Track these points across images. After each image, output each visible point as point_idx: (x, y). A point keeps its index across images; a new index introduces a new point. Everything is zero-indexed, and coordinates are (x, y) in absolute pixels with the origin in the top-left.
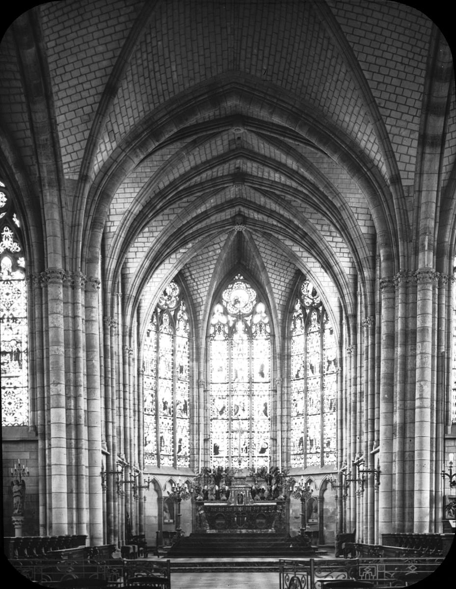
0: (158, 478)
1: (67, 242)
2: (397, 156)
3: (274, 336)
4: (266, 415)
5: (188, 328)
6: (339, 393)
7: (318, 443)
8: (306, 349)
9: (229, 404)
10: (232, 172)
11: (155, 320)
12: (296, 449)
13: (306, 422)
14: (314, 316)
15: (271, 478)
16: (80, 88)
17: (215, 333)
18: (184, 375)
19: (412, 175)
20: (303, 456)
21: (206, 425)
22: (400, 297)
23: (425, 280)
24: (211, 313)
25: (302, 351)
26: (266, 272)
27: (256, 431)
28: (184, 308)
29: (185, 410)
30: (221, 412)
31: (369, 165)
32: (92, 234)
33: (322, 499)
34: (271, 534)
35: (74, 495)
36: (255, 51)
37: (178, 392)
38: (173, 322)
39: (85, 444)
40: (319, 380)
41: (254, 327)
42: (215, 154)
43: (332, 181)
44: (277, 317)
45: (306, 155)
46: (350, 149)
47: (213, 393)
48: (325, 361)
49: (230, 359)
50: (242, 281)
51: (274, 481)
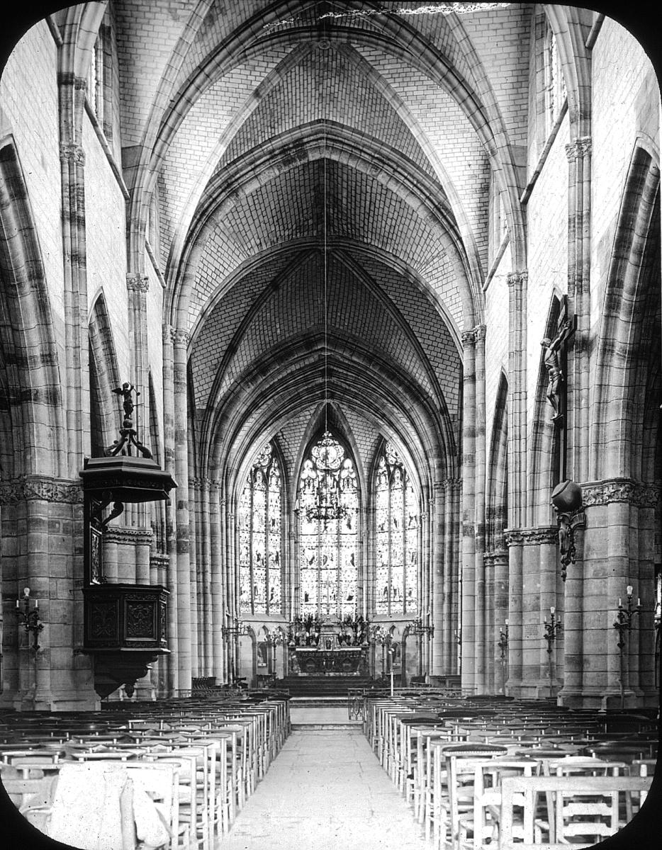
1: (197, 456)
2: (445, 394)
3: (360, 490)
4: (353, 564)
5: (279, 483)
6: (419, 547)
8: (390, 504)
9: (319, 554)
12: (380, 597)
13: (390, 573)
14: (397, 474)
15: (356, 626)
16: (210, 349)
17: (305, 487)
18: (276, 527)
19: (456, 407)
20: (387, 604)
21: (297, 575)
24: (302, 469)
25: (387, 506)
26: (353, 435)
27: (344, 580)
28: (276, 465)
29: (277, 560)
31: (425, 396)
33: (404, 644)
34: (356, 677)
35: (203, 646)
36: (339, 314)
37: (270, 544)
38: (266, 479)
39: (210, 607)
40: (402, 534)
41: (342, 481)
44: (363, 474)
46: (411, 384)
47: (303, 544)
48: (407, 516)
50: (330, 437)
51: (359, 629)
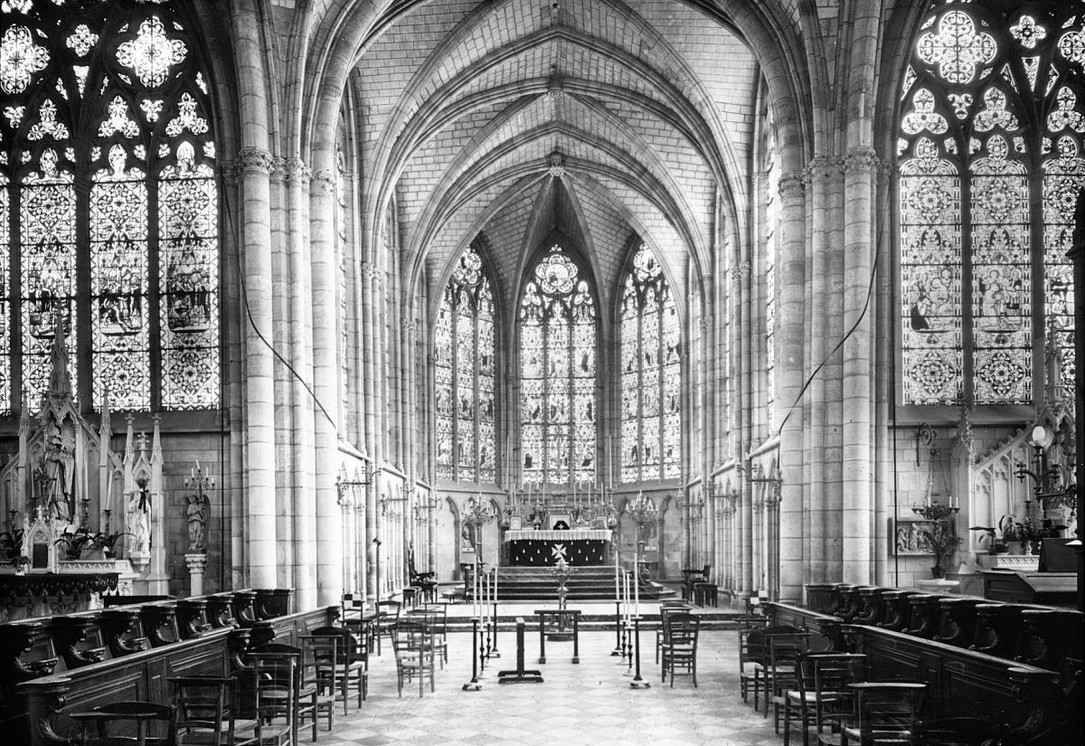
0: (453, 496)
1: (276, 108)
4: (590, 418)
7: (655, 453)
8: (640, 334)
10: (546, 73)
11: (450, 298)
14: (651, 294)
17: (527, 316)
22: (815, 199)
23: (860, 166)
24: (522, 293)
30: (535, 416)
32: (322, 105)
38: (474, 301)
40: (657, 373)
42: (521, 31)
43: (690, 62)
44: (604, 295)
45: (653, 22)
48: (665, 348)
49: (545, 349)
50: (559, 253)
